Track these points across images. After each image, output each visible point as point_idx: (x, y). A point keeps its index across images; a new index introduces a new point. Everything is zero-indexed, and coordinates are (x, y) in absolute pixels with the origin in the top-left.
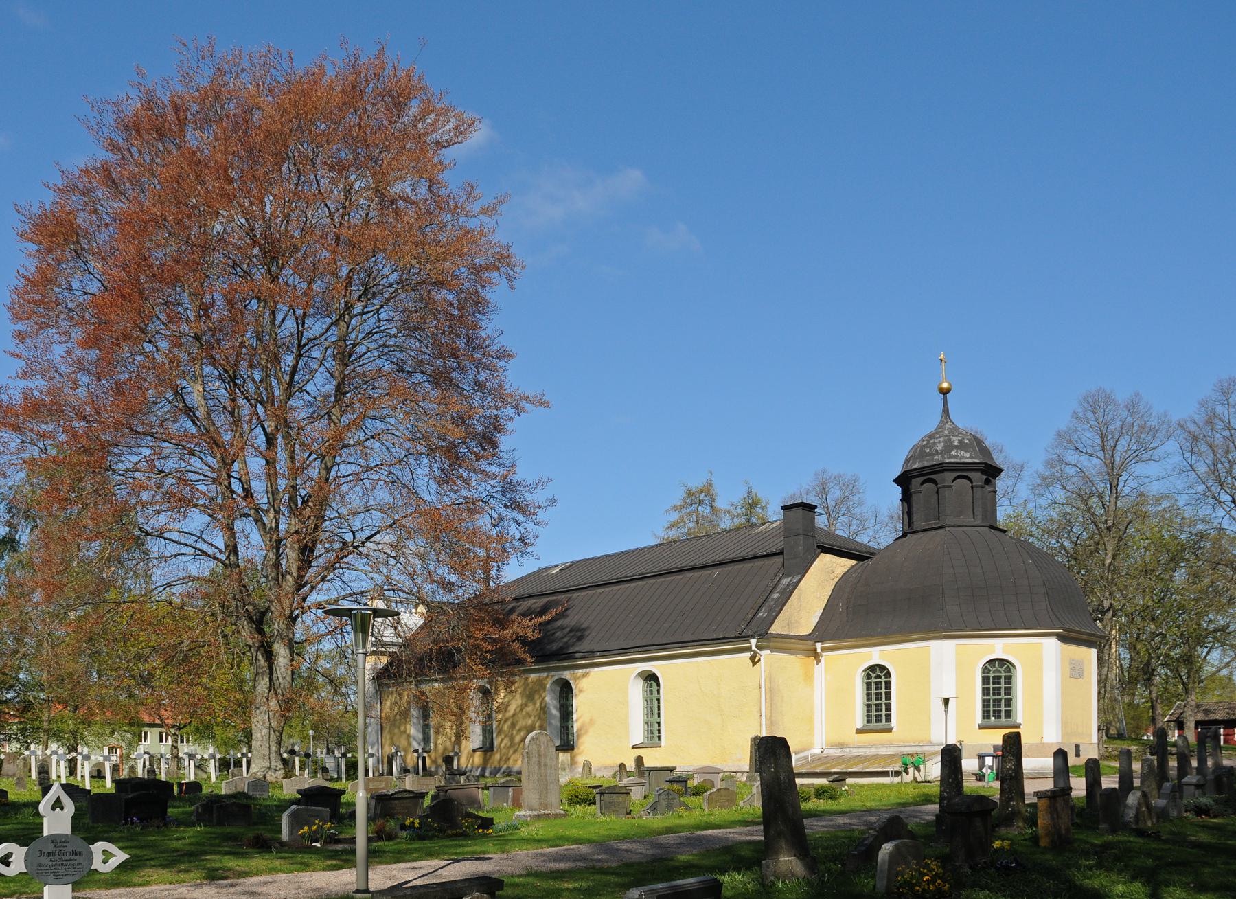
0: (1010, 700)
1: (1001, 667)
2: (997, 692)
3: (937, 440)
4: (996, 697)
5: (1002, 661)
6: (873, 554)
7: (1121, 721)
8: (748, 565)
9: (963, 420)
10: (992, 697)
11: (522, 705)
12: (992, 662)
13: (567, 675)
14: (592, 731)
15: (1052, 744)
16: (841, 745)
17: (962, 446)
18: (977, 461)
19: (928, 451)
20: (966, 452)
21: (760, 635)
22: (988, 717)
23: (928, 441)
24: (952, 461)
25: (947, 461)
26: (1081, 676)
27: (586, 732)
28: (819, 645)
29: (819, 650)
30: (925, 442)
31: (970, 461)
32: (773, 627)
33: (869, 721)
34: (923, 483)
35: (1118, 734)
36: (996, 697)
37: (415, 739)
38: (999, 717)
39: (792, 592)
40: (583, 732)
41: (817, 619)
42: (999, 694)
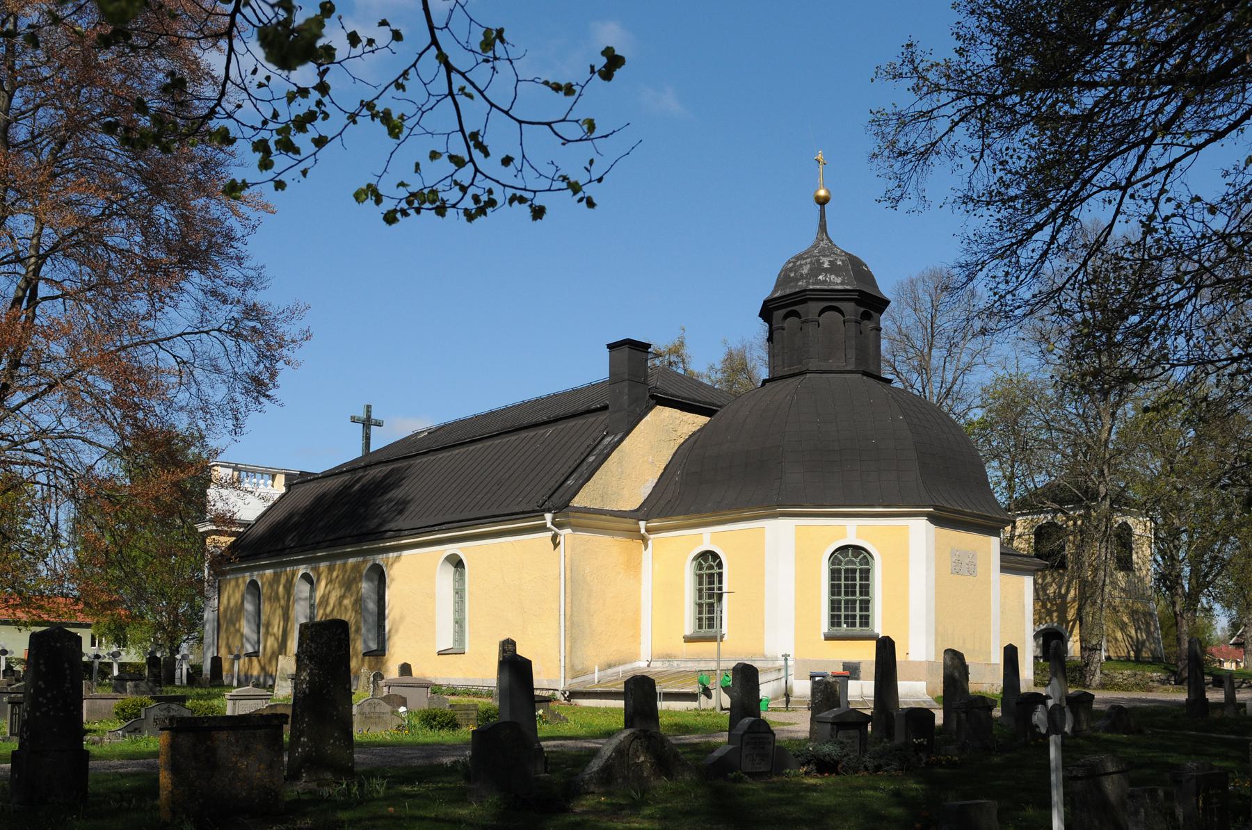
0: (868, 602)
1: (856, 557)
2: (850, 590)
3: (803, 262)
4: (850, 598)
5: (857, 549)
6: (720, 407)
7: (1157, 641)
8: (580, 422)
9: (847, 239)
10: (843, 597)
11: (340, 597)
12: (843, 549)
13: (380, 559)
14: (402, 629)
15: (920, 663)
16: (667, 657)
17: (834, 269)
18: (849, 287)
19: (792, 275)
20: (837, 276)
21: (556, 509)
22: (839, 625)
23: (795, 263)
24: (818, 287)
25: (811, 287)
26: (972, 572)
27: (397, 631)
28: (642, 524)
29: (643, 531)
30: (791, 265)
31: (840, 287)
32: (576, 499)
33: (700, 627)
34: (786, 316)
35: (1154, 658)
36: (850, 598)
37: (248, 640)
38: (854, 625)
39: (608, 455)
40: (393, 632)
41: (649, 491)
42: (854, 593)
